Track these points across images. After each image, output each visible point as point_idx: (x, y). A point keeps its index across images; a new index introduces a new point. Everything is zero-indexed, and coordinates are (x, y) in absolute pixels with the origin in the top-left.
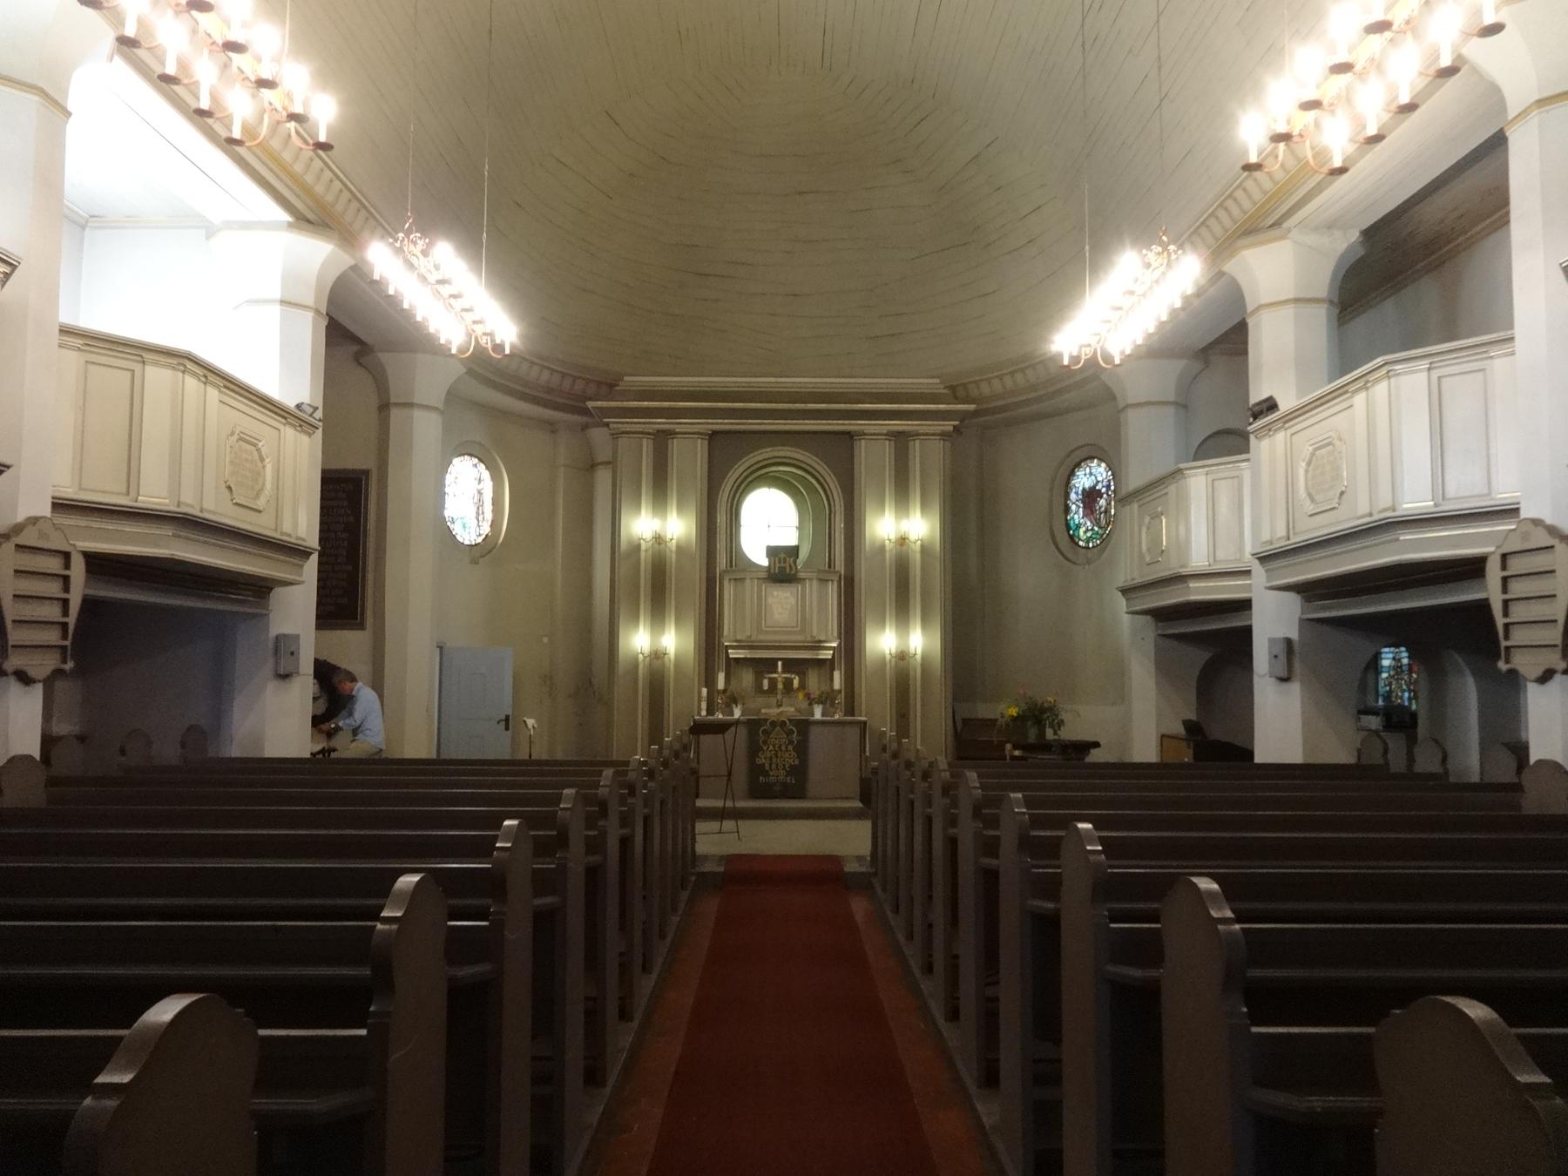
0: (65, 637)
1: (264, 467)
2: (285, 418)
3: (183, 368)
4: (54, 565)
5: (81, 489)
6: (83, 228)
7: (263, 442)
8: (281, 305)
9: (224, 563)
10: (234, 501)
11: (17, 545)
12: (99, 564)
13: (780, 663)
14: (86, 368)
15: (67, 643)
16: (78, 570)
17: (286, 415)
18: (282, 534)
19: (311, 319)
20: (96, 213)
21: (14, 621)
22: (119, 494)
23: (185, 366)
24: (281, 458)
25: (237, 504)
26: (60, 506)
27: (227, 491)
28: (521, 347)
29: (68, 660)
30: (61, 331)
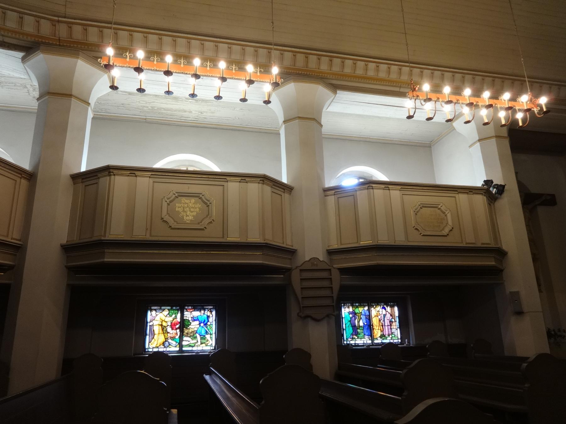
0: (333, 302)
1: (446, 215)
2: (456, 191)
3: (371, 187)
4: (325, 275)
5: (341, 244)
6: (430, 147)
7: (441, 205)
8: (479, 142)
9: (444, 263)
10: (422, 234)
11: (300, 270)
12: (343, 271)
13: (341, 283)
14: (402, 196)
15: (334, 304)
16: (336, 276)
17: (457, 189)
18: (467, 243)
19: (495, 141)
20: (431, 140)
21: (302, 298)
22: (281, 243)
23: (372, 186)
24: (459, 208)
25: (423, 235)
26: (331, 253)
27: (416, 231)
28: (524, 113)
29: (335, 311)
30: (324, 191)
